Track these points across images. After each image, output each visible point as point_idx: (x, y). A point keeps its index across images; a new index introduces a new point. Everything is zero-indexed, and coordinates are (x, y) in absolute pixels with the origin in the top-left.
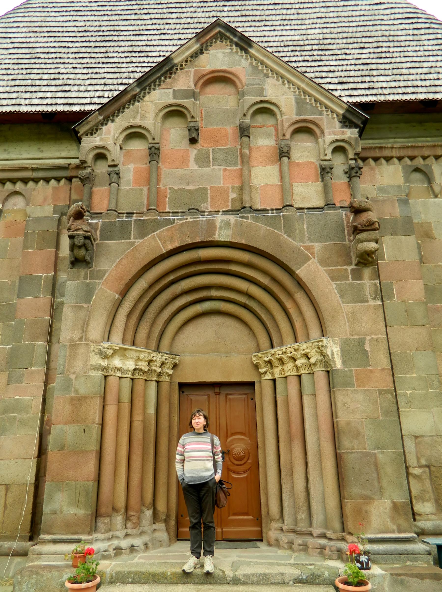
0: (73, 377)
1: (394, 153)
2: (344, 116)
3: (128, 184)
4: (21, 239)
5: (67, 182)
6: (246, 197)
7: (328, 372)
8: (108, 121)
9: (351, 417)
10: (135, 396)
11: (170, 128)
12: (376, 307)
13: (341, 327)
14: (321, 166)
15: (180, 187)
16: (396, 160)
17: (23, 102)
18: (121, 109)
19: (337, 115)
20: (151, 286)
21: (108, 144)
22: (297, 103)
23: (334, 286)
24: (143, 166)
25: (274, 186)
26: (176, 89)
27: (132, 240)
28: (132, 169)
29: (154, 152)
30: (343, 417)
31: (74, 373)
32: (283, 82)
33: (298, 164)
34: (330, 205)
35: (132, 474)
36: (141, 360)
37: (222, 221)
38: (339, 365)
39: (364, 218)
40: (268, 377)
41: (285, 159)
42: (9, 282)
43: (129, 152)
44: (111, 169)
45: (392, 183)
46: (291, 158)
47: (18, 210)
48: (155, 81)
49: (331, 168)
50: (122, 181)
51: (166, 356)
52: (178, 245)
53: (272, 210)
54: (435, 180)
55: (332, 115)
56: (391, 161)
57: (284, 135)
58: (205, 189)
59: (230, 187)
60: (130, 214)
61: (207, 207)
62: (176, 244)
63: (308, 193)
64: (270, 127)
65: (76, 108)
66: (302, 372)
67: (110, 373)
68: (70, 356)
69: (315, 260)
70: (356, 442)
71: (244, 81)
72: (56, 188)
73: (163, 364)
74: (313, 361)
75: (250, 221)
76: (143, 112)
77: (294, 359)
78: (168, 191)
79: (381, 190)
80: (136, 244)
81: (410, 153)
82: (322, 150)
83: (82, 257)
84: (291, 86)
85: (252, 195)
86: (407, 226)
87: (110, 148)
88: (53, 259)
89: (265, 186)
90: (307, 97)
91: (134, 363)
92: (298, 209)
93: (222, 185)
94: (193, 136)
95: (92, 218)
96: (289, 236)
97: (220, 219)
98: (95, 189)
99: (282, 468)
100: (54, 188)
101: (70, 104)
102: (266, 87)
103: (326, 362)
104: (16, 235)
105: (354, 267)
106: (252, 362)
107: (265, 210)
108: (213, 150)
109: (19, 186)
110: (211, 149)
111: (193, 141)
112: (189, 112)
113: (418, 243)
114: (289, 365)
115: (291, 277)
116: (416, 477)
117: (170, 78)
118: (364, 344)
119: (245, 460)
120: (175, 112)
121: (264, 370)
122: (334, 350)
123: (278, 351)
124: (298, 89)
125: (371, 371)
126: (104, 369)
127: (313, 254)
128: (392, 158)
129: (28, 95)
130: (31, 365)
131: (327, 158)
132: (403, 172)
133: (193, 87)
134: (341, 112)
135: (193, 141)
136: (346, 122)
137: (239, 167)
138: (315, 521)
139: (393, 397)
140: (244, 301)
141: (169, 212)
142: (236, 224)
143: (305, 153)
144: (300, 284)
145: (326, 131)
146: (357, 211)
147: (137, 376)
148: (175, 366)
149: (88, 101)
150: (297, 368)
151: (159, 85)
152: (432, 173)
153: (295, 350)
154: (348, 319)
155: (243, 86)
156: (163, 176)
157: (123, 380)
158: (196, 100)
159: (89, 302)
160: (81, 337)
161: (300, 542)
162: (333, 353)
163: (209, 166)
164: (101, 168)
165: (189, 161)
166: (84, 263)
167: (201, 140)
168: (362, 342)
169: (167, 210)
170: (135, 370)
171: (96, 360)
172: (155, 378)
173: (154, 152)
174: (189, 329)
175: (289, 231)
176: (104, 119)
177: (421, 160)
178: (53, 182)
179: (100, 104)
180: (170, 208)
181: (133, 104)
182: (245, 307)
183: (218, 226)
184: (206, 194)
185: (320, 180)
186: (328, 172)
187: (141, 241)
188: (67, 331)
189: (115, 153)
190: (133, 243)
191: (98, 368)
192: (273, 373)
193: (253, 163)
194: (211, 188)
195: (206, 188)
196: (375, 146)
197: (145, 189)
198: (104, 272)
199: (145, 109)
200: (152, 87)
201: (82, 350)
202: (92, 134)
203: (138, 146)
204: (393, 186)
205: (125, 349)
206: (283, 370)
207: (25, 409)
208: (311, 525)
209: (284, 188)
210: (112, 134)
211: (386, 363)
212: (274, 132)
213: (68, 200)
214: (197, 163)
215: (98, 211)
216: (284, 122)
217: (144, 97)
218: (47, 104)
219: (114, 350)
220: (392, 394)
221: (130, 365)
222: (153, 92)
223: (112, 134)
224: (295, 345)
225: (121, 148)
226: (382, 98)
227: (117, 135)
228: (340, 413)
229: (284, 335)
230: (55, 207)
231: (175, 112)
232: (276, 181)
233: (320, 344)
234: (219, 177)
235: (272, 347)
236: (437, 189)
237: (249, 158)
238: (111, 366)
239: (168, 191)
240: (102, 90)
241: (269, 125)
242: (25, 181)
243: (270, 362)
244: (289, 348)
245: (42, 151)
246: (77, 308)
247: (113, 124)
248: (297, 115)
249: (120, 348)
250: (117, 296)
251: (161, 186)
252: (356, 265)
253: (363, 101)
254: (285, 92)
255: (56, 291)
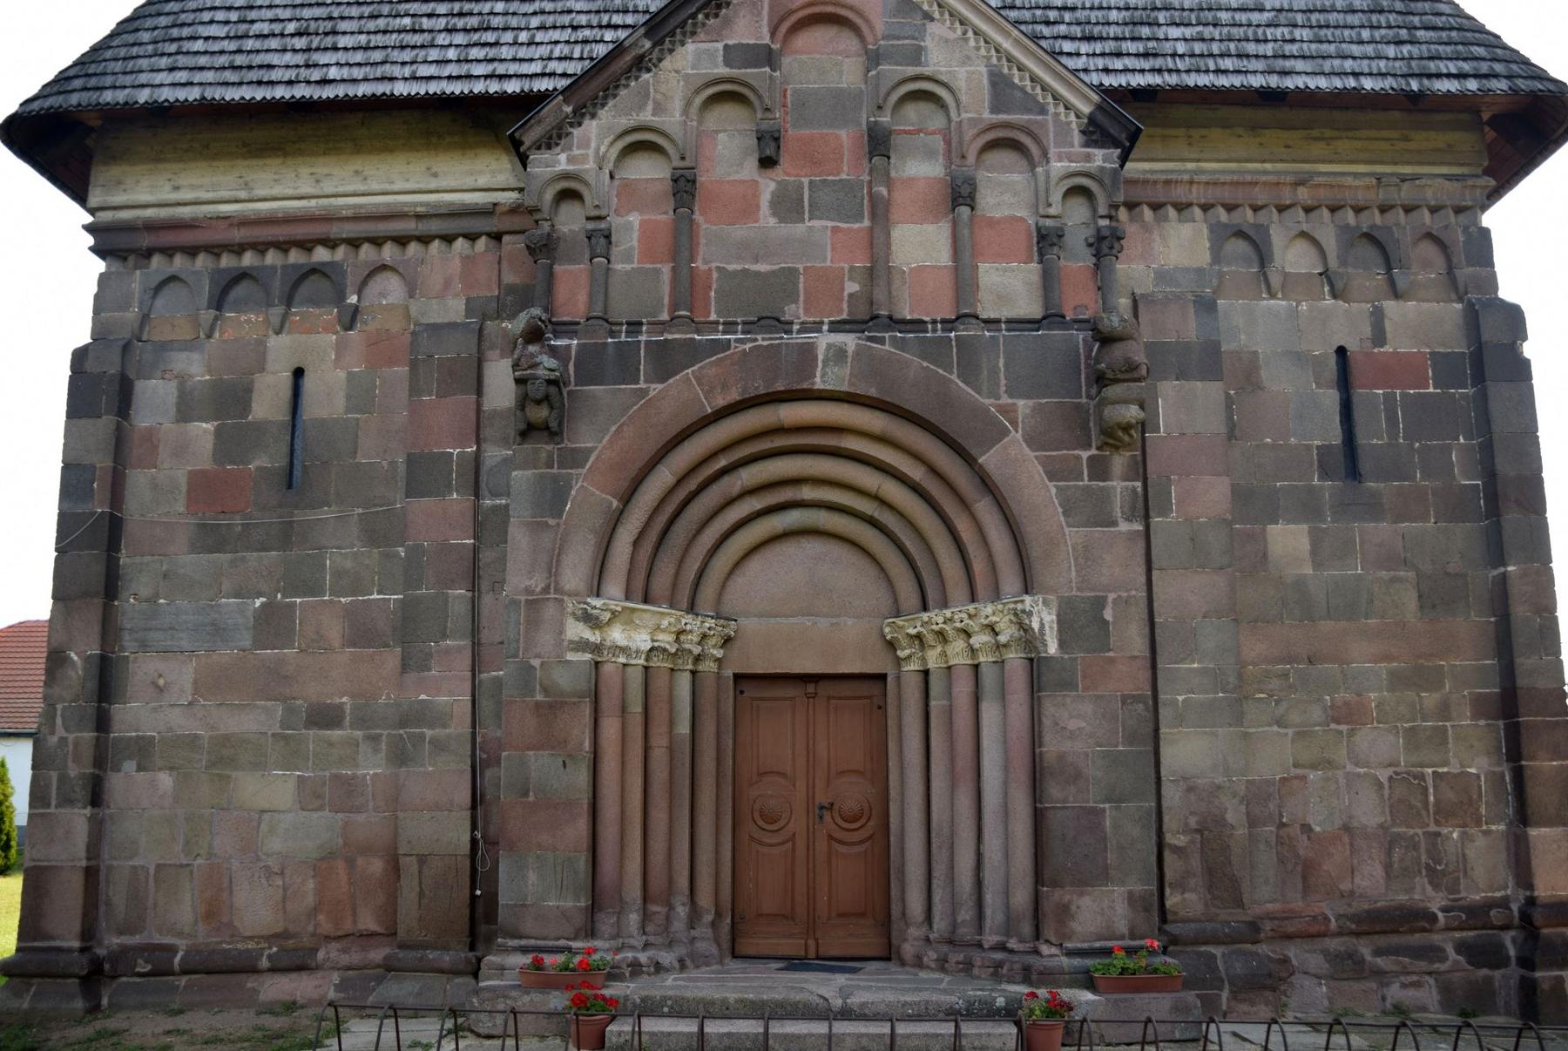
0: (536, 663)
1: (1196, 195)
2: (1091, 119)
3: (629, 260)
4: (403, 370)
5: (493, 243)
6: (880, 295)
7: (1031, 660)
8: (583, 115)
9: (1067, 746)
10: (652, 701)
11: (717, 132)
12: (1131, 535)
13: (1063, 574)
14: (1039, 229)
15: (738, 267)
16: (1197, 211)
17: (397, 71)
18: (610, 90)
19: (1078, 117)
20: (680, 482)
21: (586, 171)
22: (993, 84)
23: (1054, 491)
24: (663, 217)
25: (940, 268)
26: (730, 42)
27: (642, 385)
28: (637, 225)
29: (684, 187)
30: (1052, 746)
31: (538, 656)
32: (965, 33)
33: (992, 223)
34: (1052, 318)
35: (651, 843)
36: (663, 631)
37: (829, 346)
38: (1052, 648)
39: (1118, 351)
40: (914, 666)
41: (964, 211)
42: (385, 463)
43: (628, 185)
44: (591, 226)
45: (1186, 263)
46: (978, 207)
47: (390, 308)
48: (683, 24)
49: (1060, 237)
50: (615, 251)
51: (710, 623)
52: (738, 398)
53: (934, 322)
54: (1272, 261)
55: (1067, 115)
56: (1186, 213)
57: (963, 157)
58: (793, 272)
59: (846, 266)
60: (634, 326)
61: (796, 312)
62: (734, 395)
63: (1009, 286)
64: (933, 133)
65: (512, 87)
66: (982, 659)
67: (606, 656)
68: (528, 622)
69: (1019, 436)
70: (1073, 789)
71: (880, 27)
72: (468, 257)
73: (704, 636)
74: (1003, 639)
75: (887, 347)
76: (659, 97)
77: (967, 634)
78: (715, 275)
79: (1162, 276)
80: (652, 393)
81: (1227, 195)
82: (1042, 194)
83: (544, 417)
84: (982, 43)
85: (894, 287)
86: (1207, 361)
87: (591, 179)
88: (473, 416)
89: (921, 269)
90: (1015, 71)
91: (648, 637)
92: (986, 321)
93: (829, 263)
94: (768, 152)
95: (557, 335)
96: (967, 384)
97: (824, 341)
98: (557, 268)
99: (933, 835)
100: (467, 260)
101: (501, 77)
102: (928, 43)
103: (1029, 640)
104: (392, 362)
105: (1094, 452)
106: (883, 636)
107: (918, 325)
108: (811, 182)
109: (389, 252)
110: (806, 181)
111: (767, 163)
112: (760, 97)
113: (1227, 395)
114: (959, 645)
115: (967, 468)
116: (1177, 850)
117: (717, 16)
118: (1104, 607)
119: (863, 821)
120: (727, 95)
121: (907, 652)
122: (1044, 617)
123: (936, 617)
124: (997, 51)
125: (1112, 661)
126: (596, 648)
127: (1014, 423)
128: (1190, 205)
129: (407, 56)
130: (444, 636)
131: (1052, 211)
132: (1210, 240)
133: (767, 40)
134: (1086, 109)
135: (767, 163)
136: (1095, 133)
137: (866, 223)
138: (988, 923)
139: (1147, 709)
140: (869, 513)
141: (717, 323)
142: (858, 353)
143: (1007, 197)
144: (986, 484)
145: (1052, 151)
146: (1106, 339)
147: (655, 662)
148: (727, 641)
149: (536, 68)
150: (973, 651)
151: (693, 33)
152: (1269, 243)
153: (970, 617)
154: (1076, 559)
155: (876, 41)
156: (703, 241)
157: (629, 669)
158: (774, 70)
159: (560, 516)
160: (548, 587)
161: (961, 957)
162: (1042, 625)
163: (803, 221)
164: (570, 221)
165: (758, 207)
166: (546, 433)
167: (784, 160)
168: (1100, 603)
169: (713, 317)
170: (652, 649)
171: (576, 630)
172: (690, 667)
173: (684, 187)
174: (755, 565)
175: (969, 372)
176: (574, 112)
177: (1249, 212)
178: (460, 243)
179: (564, 75)
180: (718, 313)
181: (637, 78)
182: (872, 522)
183: (820, 357)
184: (796, 284)
185: (1036, 257)
186: (1053, 245)
187: (660, 386)
188: (521, 578)
189: (599, 187)
190: (645, 392)
191: (583, 645)
192: (923, 659)
193: (895, 214)
194: (806, 268)
195: (796, 270)
196: (1155, 177)
197: (666, 269)
198: (590, 451)
199: (663, 88)
200: (678, 37)
201: (550, 611)
202: (549, 147)
203: (649, 171)
204: (1186, 270)
205: (633, 610)
206: (944, 654)
207: (438, 718)
208: (980, 929)
209: (963, 279)
210: (593, 145)
211: (1139, 645)
212: (941, 145)
213: (495, 286)
214: (774, 214)
215: (565, 319)
216: (965, 126)
217: (660, 60)
218: (450, 77)
219: (613, 612)
220: (1146, 704)
221: (642, 640)
222: (680, 50)
223: (593, 145)
224: (971, 608)
225: (612, 177)
226: (1172, 80)
227: (603, 149)
228: (1048, 737)
229: (950, 584)
230: (468, 301)
231: (727, 95)
232: (944, 258)
233: (1019, 607)
234: (823, 245)
235: (925, 608)
236: (1275, 280)
237: (888, 203)
238: (608, 643)
239: (715, 275)
240: (567, 42)
241: (932, 128)
242: (402, 241)
243: (919, 637)
244: (959, 613)
245: (435, 175)
246: (537, 527)
247: (594, 123)
248: (992, 112)
249: (624, 608)
250: (615, 503)
251: (699, 264)
252: (1098, 448)
253: (1134, 84)
254: (968, 58)
255: (483, 485)
